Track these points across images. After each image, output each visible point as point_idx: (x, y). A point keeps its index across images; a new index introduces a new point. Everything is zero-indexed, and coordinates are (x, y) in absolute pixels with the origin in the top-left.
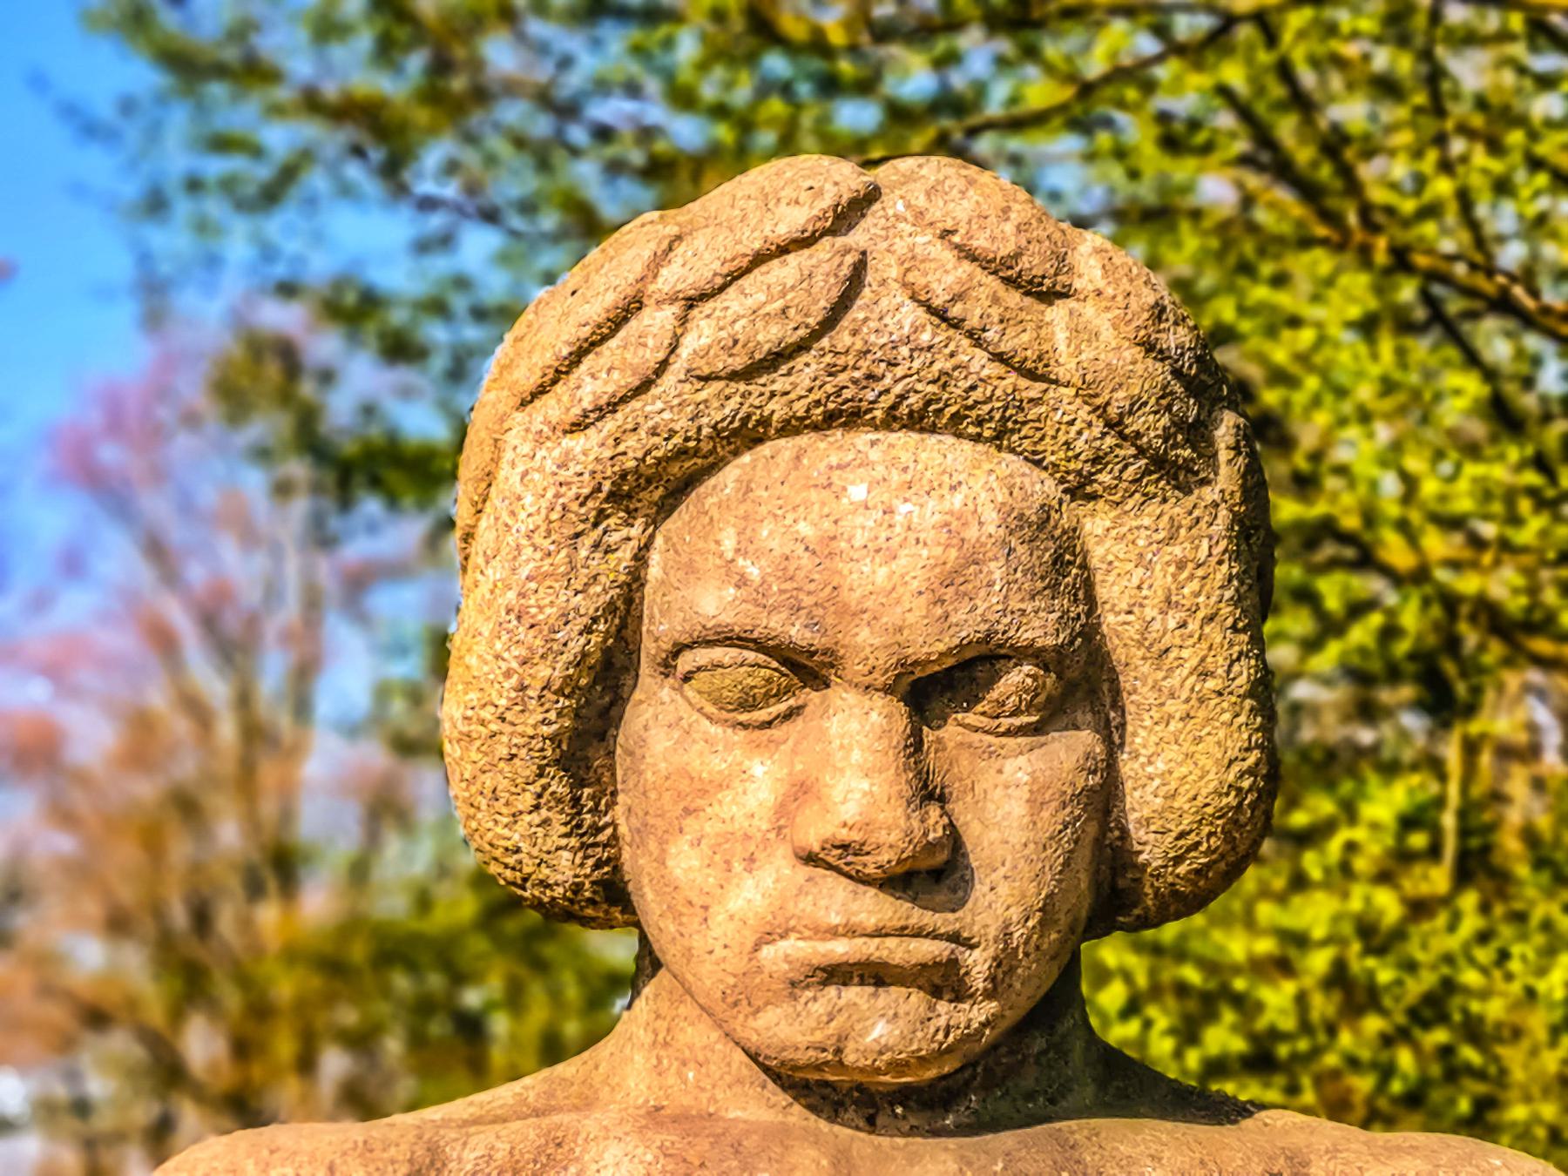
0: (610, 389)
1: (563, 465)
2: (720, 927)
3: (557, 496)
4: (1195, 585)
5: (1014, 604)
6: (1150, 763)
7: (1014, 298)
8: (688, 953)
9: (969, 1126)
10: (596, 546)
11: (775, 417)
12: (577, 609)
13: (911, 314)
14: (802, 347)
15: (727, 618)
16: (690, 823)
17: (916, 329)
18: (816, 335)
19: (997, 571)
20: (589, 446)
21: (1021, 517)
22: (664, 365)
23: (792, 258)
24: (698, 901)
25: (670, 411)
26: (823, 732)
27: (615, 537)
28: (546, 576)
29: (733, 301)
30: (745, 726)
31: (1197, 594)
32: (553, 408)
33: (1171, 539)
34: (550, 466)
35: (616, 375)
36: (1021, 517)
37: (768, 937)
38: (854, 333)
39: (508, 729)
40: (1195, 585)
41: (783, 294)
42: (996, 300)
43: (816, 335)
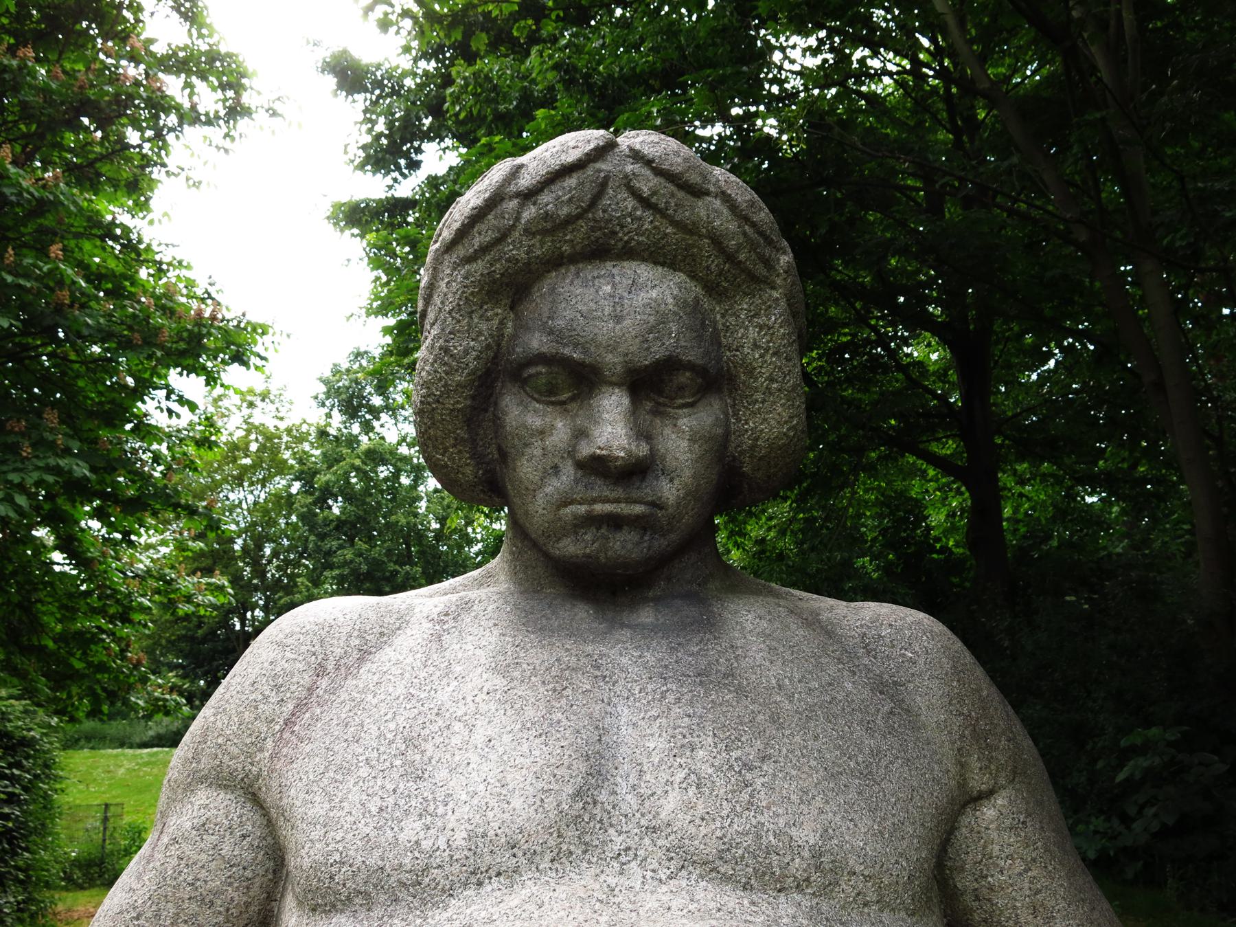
0: (488, 239)
1: (466, 278)
2: (540, 500)
3: (463, 292)
4: (768, 338)
5: (682, 343)
6: (747, 423)
7: (681, 194)
8: (526, 513)
9: (726, 448)
10: (481, 316)
11: (812, 41)
12: (473, 348)
13: (630, 203)
14: (579, 217)
15: (544, 350)
16: (528, 450)
17: (635, 209)
18: (586, 211)
19: (674, 328)
20: (479, 266)
21: (685, 301)
22: (513, 227)
23: (575, 175)
24: (531, 487)
25: (516, 250)
26: (591, 405)
27: (489, 314)
28: (459, 331)
29: (546, 197)
30: (553, 403)
31: (768, 342)
32: (461, 251)
33: (757, 315)
34: (459, 279)
35: (490, 232)
36: (685, 301)
37: (566, 503)
38: (604, 211)
39: (440, 406)
40: (768, 338)
41: (570, 191)
42: (673, 195)
43: (586, 211)
